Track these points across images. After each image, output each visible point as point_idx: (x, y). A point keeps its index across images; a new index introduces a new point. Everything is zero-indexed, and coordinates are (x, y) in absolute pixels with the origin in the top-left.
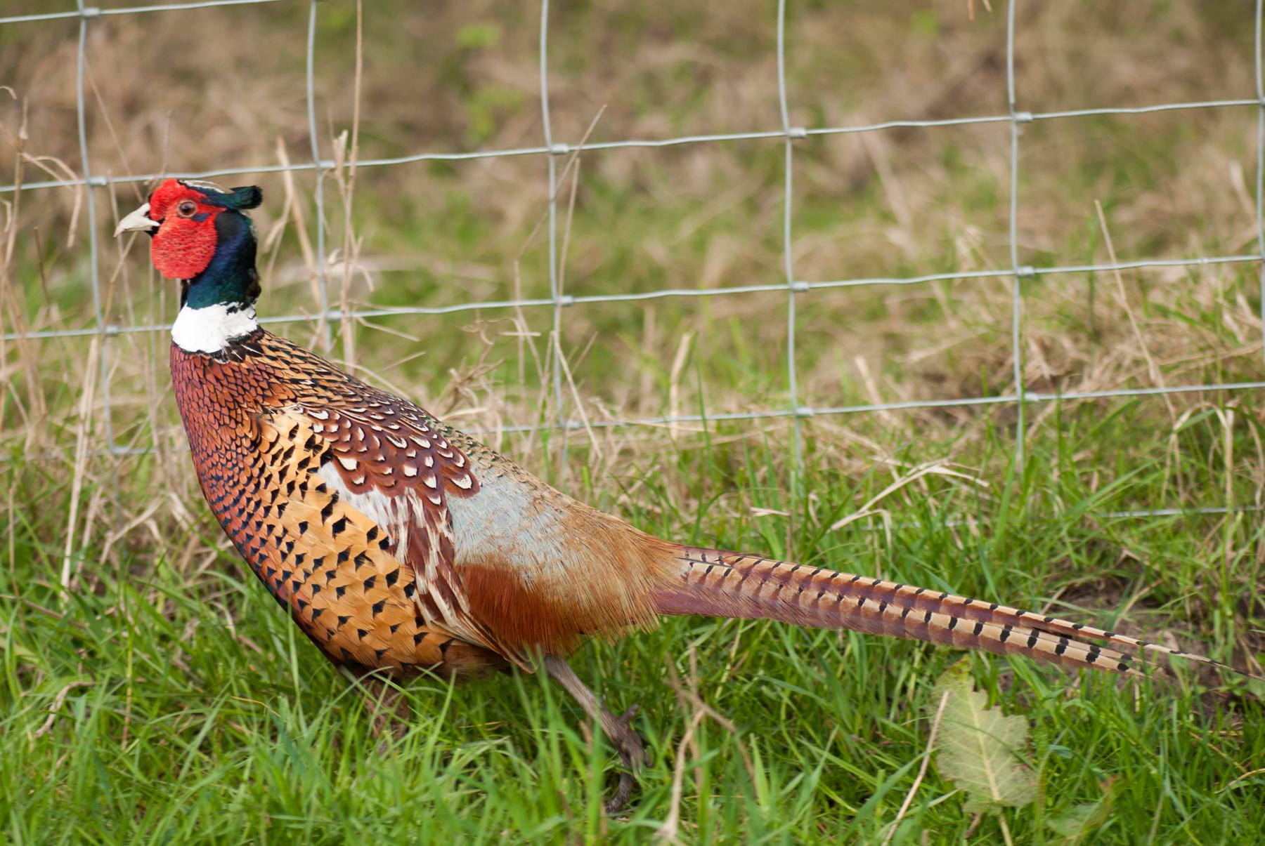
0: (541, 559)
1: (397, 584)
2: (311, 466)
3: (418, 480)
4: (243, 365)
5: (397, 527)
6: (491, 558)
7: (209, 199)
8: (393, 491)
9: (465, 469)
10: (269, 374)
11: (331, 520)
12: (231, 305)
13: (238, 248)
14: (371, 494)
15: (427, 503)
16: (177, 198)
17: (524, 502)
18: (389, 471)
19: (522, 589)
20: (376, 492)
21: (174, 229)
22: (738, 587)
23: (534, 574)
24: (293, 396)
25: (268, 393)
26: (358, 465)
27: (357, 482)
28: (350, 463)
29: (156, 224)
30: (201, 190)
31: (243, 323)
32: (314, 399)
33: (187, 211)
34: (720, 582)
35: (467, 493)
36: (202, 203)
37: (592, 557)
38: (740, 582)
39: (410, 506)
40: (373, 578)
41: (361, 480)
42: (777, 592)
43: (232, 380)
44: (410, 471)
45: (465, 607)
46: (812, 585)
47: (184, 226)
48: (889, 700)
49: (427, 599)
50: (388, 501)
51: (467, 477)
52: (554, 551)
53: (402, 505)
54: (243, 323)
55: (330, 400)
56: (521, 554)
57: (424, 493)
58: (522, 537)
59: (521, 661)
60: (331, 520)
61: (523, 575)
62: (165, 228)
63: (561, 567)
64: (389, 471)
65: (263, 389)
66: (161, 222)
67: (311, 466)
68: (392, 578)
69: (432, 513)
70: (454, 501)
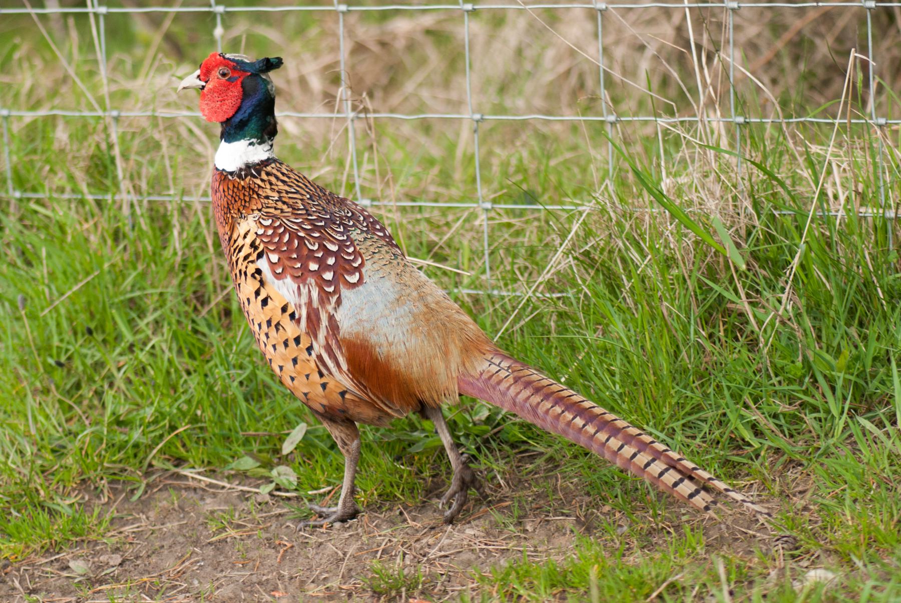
0: (391, 339)
1: (301, 346)
2: (251, 259)
3: (318, 274)
4: (242, 183)
5: (300, 306)
6: (357, 334)
7: (238, 66)
8: (299, 280)
9: (358, 269)
10: (253, 191)
11: (260, 298)
12: (253, 140)
13: (259, 100)
14: (286, 280)
15: (321, 289)
16: (217, 66)
17: (392, 297)
18: (299, 265)
19: (377, 359)
20: (289, 280)
21: (215, 87)
22: (508, 388)
23: (385, 349)
24: (260, 207)
25: (247, 204)
26: (279, 259)
27: (278, 271)
28: (274, 258)
29: (204, 84)
30: (233, 61)
31: (259, 153)
32: (272, 210)
33: (224, 75)
34: (499, 383)
35: (353, 286)
36: (234, 69)
37: (426, 342)
38: (511, 385)
39: (310, 291)
40: (287, 340)
41: (279, 270)
42: (529, 398)
43: (231, 192)
44: (313, 266)
45: (345, 367)
46: (551, 399)
47: (221, 84)
48: (183, 562)
49: (320, 357)
50: (295, 286)
51: (357, 274)
52: (401, 335)
53: (304, 291)
54: (259, 153)
55: (282, 211)
56: (377, 334)
57: (322, 284)
58: (382, 322)
59: (390, 408)
60: (260, 298)
61: (377, 349)
62: (209, 86)
63: (403, 347)
64: (299, 265)
65: (245, 201)
66: (206, 82)
67: (251, 259)
68: (297, 340)
69: (325, 297)
70: (345, 292)
